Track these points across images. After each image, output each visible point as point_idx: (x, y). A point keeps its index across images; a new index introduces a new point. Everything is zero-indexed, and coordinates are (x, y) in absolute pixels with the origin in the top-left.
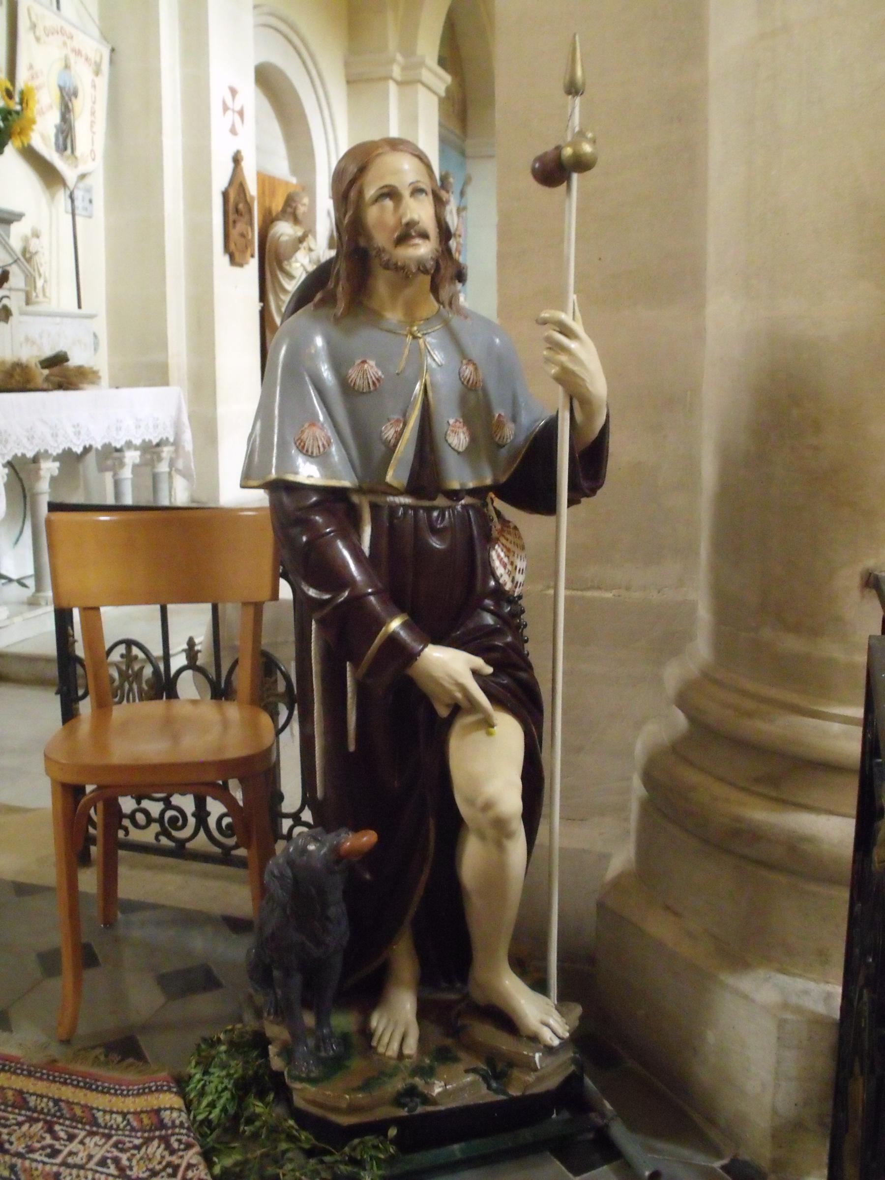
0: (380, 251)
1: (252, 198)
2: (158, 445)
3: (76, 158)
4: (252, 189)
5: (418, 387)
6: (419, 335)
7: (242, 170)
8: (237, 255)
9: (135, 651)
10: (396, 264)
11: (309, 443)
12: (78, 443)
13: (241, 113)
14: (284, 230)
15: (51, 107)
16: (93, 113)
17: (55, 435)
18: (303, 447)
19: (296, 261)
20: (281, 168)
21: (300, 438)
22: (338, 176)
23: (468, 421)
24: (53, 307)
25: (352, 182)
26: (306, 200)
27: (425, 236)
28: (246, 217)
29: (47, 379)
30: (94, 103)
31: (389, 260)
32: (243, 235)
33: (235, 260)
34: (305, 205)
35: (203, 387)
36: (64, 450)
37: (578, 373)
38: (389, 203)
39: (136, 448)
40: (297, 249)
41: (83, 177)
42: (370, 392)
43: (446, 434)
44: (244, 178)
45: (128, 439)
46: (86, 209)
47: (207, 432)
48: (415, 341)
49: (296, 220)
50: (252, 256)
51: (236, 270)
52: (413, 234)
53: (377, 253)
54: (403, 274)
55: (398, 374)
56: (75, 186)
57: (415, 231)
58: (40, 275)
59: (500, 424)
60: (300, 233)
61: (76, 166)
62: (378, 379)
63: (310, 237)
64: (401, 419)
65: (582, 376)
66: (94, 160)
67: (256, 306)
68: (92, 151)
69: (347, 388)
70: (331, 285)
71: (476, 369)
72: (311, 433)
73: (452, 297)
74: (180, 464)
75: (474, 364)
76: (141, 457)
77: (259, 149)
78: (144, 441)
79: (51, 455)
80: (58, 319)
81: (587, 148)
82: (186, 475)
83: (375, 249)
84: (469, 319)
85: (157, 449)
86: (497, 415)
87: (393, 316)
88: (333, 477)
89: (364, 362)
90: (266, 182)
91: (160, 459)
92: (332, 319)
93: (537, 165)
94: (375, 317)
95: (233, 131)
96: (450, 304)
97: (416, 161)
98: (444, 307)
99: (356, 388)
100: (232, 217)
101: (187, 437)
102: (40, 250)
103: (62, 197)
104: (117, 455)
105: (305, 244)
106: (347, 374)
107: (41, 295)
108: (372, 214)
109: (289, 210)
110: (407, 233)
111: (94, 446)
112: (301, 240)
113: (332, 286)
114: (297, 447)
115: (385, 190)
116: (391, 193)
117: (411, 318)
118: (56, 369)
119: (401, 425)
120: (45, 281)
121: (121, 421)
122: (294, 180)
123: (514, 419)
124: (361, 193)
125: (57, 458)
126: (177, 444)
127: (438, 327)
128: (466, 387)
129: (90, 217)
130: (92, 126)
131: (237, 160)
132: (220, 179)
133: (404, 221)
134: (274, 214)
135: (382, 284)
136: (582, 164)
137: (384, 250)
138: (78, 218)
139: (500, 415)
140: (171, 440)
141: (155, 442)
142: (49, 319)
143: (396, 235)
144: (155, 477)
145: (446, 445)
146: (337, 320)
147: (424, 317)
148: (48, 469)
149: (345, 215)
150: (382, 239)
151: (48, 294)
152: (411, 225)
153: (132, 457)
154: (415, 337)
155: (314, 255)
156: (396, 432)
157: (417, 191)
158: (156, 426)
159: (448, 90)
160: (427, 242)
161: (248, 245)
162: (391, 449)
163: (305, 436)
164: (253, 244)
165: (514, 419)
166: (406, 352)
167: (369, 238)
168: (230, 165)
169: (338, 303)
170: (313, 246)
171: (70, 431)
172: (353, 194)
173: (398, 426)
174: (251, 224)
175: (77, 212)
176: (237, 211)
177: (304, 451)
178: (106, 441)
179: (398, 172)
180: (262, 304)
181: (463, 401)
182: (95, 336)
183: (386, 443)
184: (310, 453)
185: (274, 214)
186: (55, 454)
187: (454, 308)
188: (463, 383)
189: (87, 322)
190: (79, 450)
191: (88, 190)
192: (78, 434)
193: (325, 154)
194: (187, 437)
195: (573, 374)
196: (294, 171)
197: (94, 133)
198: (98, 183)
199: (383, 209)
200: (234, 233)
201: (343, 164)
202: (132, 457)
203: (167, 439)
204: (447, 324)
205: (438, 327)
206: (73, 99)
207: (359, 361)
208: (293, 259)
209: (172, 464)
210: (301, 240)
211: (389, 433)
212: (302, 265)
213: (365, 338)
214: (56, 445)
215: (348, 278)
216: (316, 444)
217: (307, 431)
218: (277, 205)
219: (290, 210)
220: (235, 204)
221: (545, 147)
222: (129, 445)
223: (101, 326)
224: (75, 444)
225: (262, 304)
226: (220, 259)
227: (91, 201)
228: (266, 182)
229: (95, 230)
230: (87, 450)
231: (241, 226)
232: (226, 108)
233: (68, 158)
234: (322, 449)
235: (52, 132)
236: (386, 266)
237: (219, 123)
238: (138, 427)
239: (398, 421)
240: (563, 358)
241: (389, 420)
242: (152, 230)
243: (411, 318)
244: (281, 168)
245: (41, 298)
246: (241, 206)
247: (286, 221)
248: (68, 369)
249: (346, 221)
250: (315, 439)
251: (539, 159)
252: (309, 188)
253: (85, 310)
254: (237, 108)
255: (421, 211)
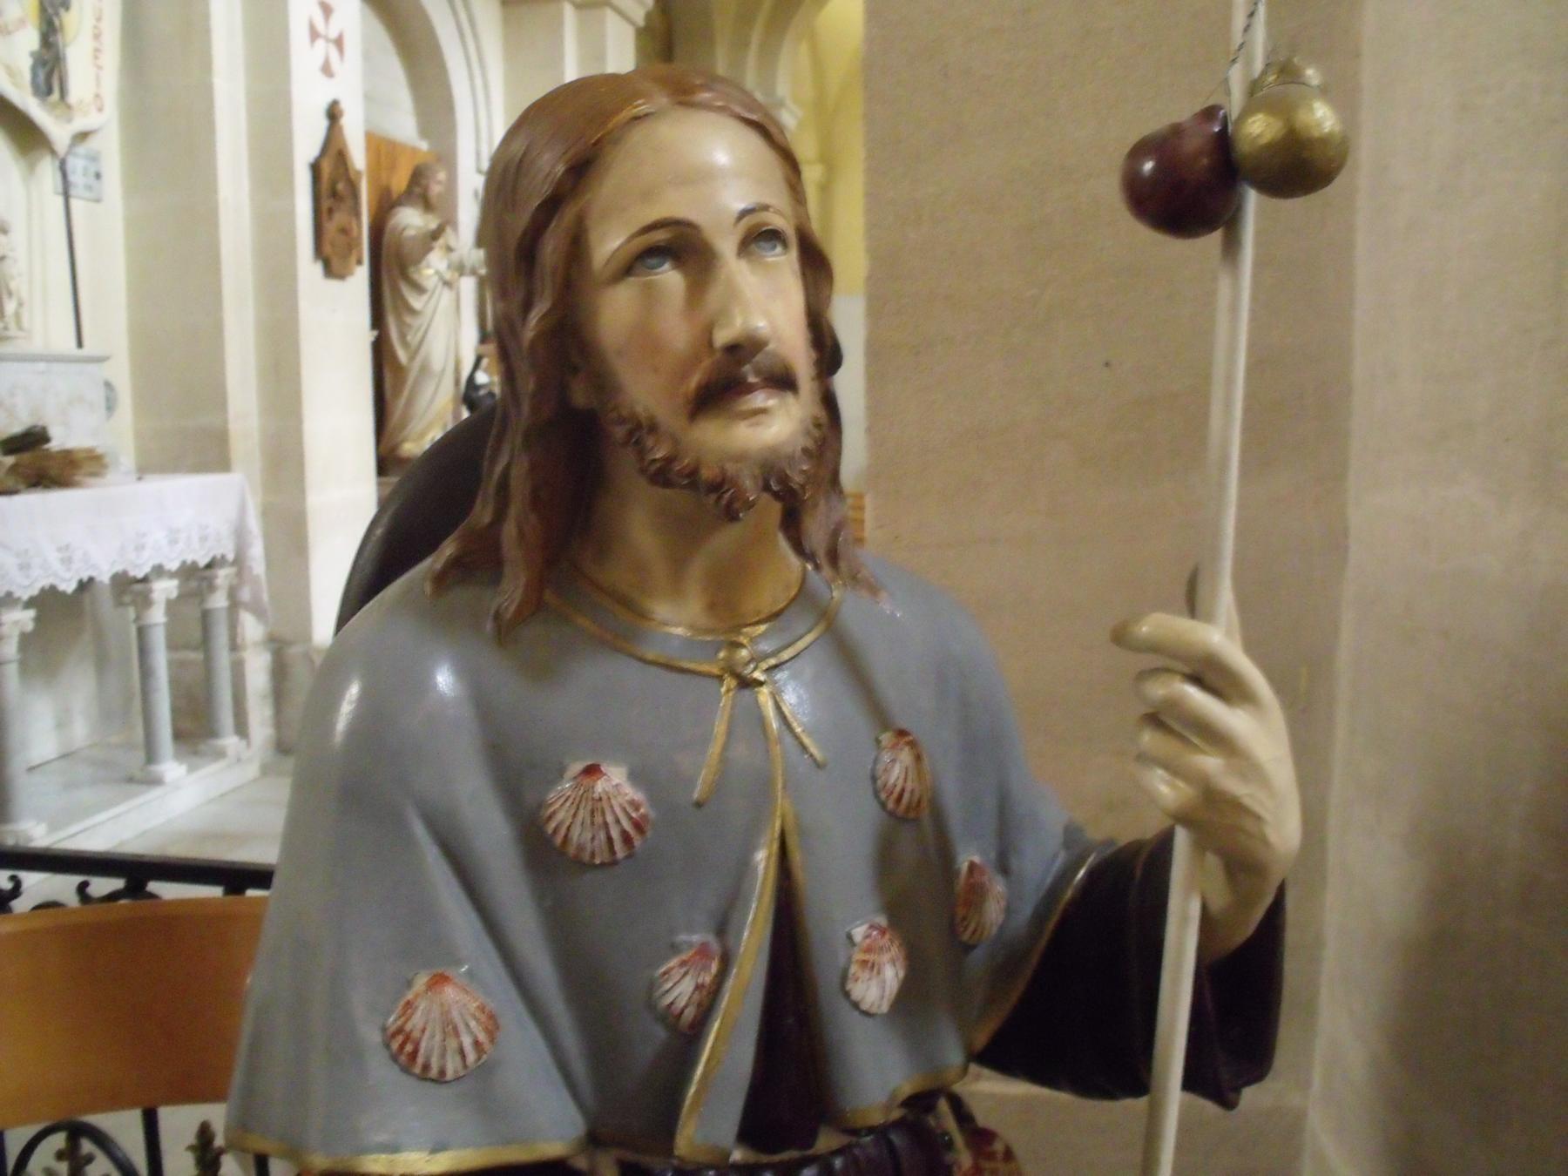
0: (642, 430)
1: (359, 173)
2: (209, 566)
3: (69, 107)
4: (358, 158)
5: (763, 858)
6: (758, 675)
7: (341, 129)
8: (335, 262)
9: (87, 1146)
10: (693, 473)
11: (430, 1045)
12: (67, 575)
13: (339, 43)
14: (410, 220)
15: (22, 22)
16: (97, 37)
17: (24, 567)
18: (413, 1055)
19: (428, 267)
20: (404, 127)
21: (400, 1031)
22: (504, 180)
23: (900, 913)
24: (36, 345)
25: (553, 204)
26: (442, 176)
27: (783, 381)
28: (349, 202)
29: (13, 469)
30: (99, 19)
31: (669, 460)
32: (344, 231)
33: (332, 268)
34: (439, 182)
35: (285, 463)
36: (43, 590)
37: (1247, 801)
38: (670, 278)
39: (172, 575)
40: (429, 249)
41: (82, 136)
42: (614, 863)
43: (844, 978)
44: (344, 144)
45: (156, 561)
46: (89, 188)
47: (289, 530)
48: (747, 692)
49: (427, 205)
50: (359, 262)
51: (334, 284)
52: (752, 379)
53: (631, 433)
54: (710, 497)
55: (699, 805)
56: (68, 153)
57: (758, 372)
58: (10, 294)
59: (976, 894)
60: (433, 225)
61: (69, 120)
62: (638, 826)
63: (449, 230)
64: (715, 946)
65: (1257, 808)
66: (100, 110)
67: (366, 336)
68: (97, 96)
69: (542, 852)
70: (482, 513)
71: (918, 758)
72: (436, 1014)
73: (835, 534)
74: (245, 595)
75: (913, 744)
76: (180, 587)
77: (368, 98)
78: (184, 563)
79: (19, 599)
80: (42, 366)
81: (1322, 117)
82: (259, 613)
83: (622, 421)
84: (883, 595)
85: (208, 573)
86: (964, 867)
87: (676, 619)
88: (507, 1142)
89: (592, 771)
90: (381, 147)
91: (212, 588)
92: (489, 626)
93: (1148, 166)
94: (620, 623)
95: (327, 70)
96: (834, 556)
97: (753, 140)
98: (817, 567)
99: (571, 850)
100: (326, 203)
101: (256, 551)
102: (10, 254)
103: (47, 169)
104: (139, 587)
105: (441, 241)
106: (541, 805)
107: (12, 325)
108: (616, 312)
109: (417, 190)
110: (728, 378)
111: (98, 579)
112: (435, 235)
113: (486, 518)
114: (394, 1058)
115: (660, 236)
116: (681, 246)
117: (727, 612)
118: (26, 457)
119: (714, 967)
120: (20, 304)
121: (144, 535)
122: (424, 146)
123: (1004, 869)
124: (577, 246)
125: (31, 603)
126: (239, 562)
127: (809, 638)
128: (892, 814)
129: (98, 201)
130: (96, 58)
131: (333, 114)
132: (307, 143)
133: (722, 337)
134: (395, 196)
135: (640, 523)
136: (1300, 169)
137: (653, 428)
138: (74, 203)
139: (972, 866)
140: (231, 557)
141: (202, 562)
142: (28, 366)
143: (694, 381)
144: (206, 617)
145: (845, 1006)
146: (505, 632)
147: (766, 612)
148: (16, 623)
149: (527, 306)
150: (645, 391)
151: (25, 324)
152: (743, 350)
153: (165, 589)
154: (747, 684)
155: (455, 256)
156: (698, 987)
157: (758, 237)
158: (203, 539)
159: (648, 16)
160: (790, 398)
161: (352, 245)
162: (686, 1038)
163: (417, 1021)
164: (359, 244)
165: (1004, 869)
166: (720, 728)
167: (604, 383)
168: (323, 124)
169: (507, 570)
170: (452, 243)
171: (54, 558)
172: (551, 249)
173: (706, 968)
174: (357, 214)
175: (73, 192)
176: (334, 194)
177: (417, 1070)
178: (118, 568)
179: (704, 176)
180: (375, 333)
181: (885, 859)
182: (108, 385)
183: (669, 1018)
184: (434, 1072)
185: (395, 196)
186: (25, 597)
187: (843, 565)
188: (883, 805)
189: (91, 367)
190: (69, 587)
191: (94, 158)
192: (67, 561)
193: (471, 115)
194: (256, 551)
195: (1237, 806)
196: (424, 132)
197: (100, 68)
198: (110, 146)
199: (650, 296)
200: (331, 227)
201: (518, 147)
202: (165, 589)
203: (223, 557)
204: (827, 618)
205: (809, 638)
206: (62, 11)
207: (577, 767)
208: (424, 263)
209: (232, 594)
210: (435, 235)
211: (681, 990)
212: (437, 272)
213: (595, 686)
214: (26, 582)
215: (535, 502)
216: (452, 1044)
217: (422, 1005)
218: (400, 182)
219: (418, 190)
220: (331, 181)
221: (1170, 108)
222: (159, 571)
223: (120, 372)
224: (64, 580)
225: (375, 333)
226: (308, 268)
227: (98, 176)
228: (381, 147)
229: (106, 222)
230: (85, 586)
231: (340, 218)
232: (314, 35)
233: (53, 107)
234: (471, 1057)
235: (25, 64)
236: (661, 476)
237: (305, 58)
238: (173, 542)
239: (703, 952)
240: (1211, 763)
241: (675, 949)
242: (200, 217)
243: (727, 612)
244: (404, 127)
245: (13, 331)
246: (340, 186)
247: (412, 205)
248: (49, 456)
249: (531, 327)
250: (450, 1029)
251: (1159, 145)
252: (446, 157)
253: (90, 348)
254: (333, 34)
255: (764, 301)
